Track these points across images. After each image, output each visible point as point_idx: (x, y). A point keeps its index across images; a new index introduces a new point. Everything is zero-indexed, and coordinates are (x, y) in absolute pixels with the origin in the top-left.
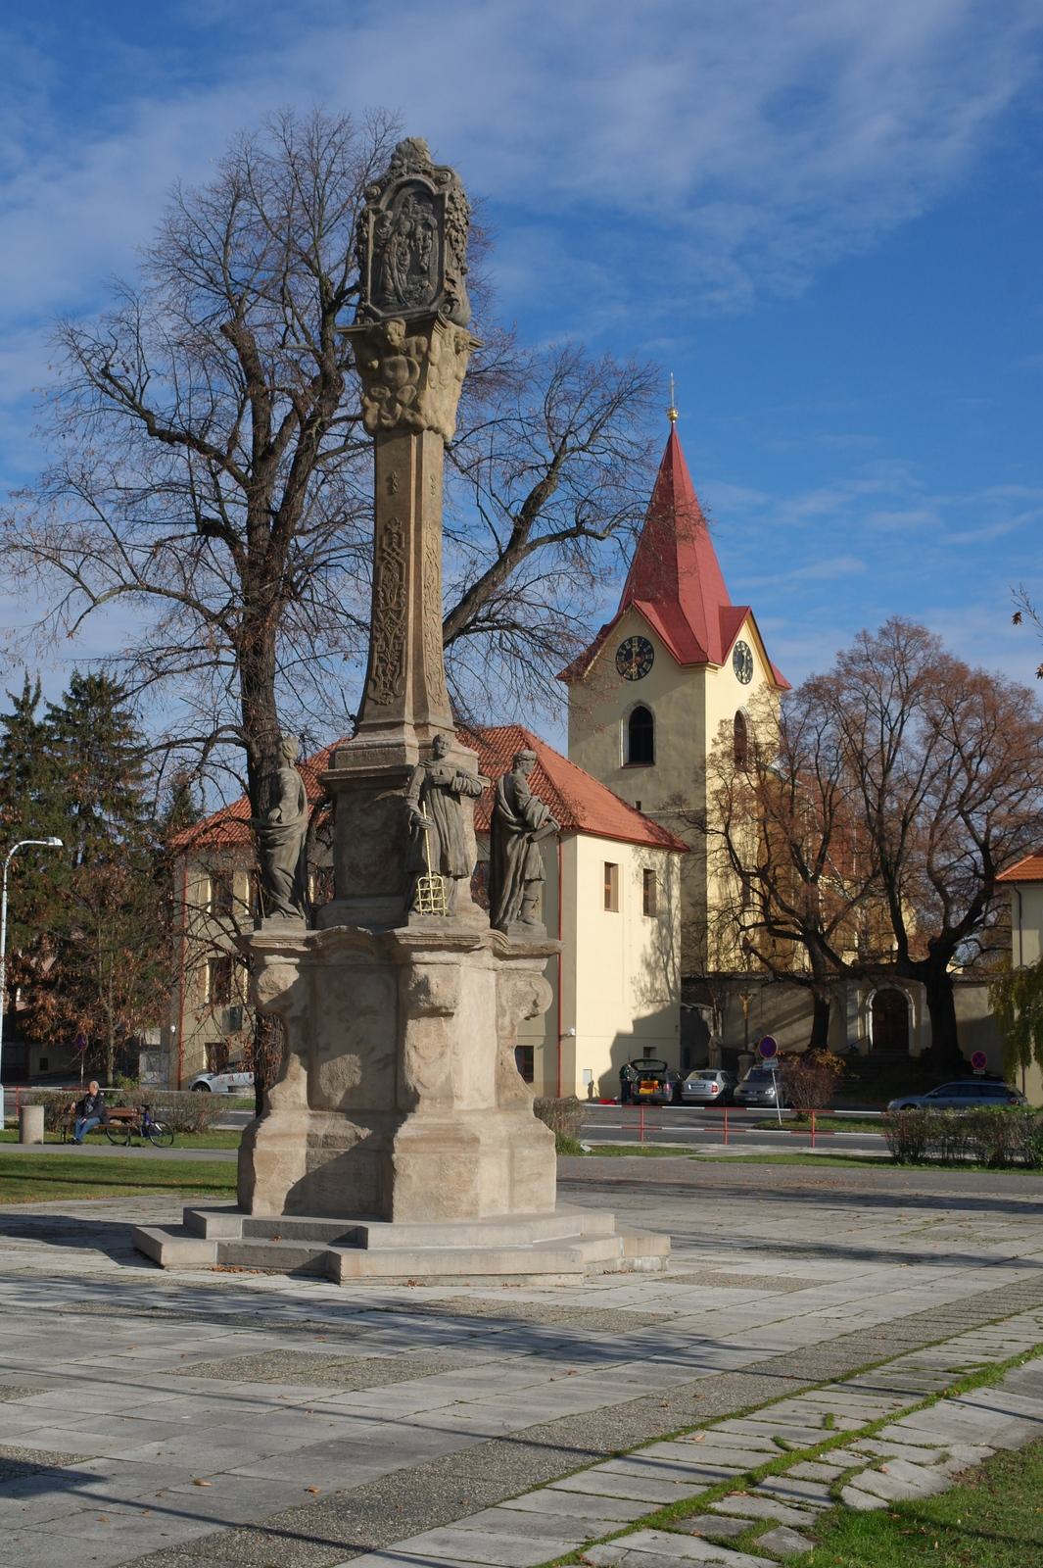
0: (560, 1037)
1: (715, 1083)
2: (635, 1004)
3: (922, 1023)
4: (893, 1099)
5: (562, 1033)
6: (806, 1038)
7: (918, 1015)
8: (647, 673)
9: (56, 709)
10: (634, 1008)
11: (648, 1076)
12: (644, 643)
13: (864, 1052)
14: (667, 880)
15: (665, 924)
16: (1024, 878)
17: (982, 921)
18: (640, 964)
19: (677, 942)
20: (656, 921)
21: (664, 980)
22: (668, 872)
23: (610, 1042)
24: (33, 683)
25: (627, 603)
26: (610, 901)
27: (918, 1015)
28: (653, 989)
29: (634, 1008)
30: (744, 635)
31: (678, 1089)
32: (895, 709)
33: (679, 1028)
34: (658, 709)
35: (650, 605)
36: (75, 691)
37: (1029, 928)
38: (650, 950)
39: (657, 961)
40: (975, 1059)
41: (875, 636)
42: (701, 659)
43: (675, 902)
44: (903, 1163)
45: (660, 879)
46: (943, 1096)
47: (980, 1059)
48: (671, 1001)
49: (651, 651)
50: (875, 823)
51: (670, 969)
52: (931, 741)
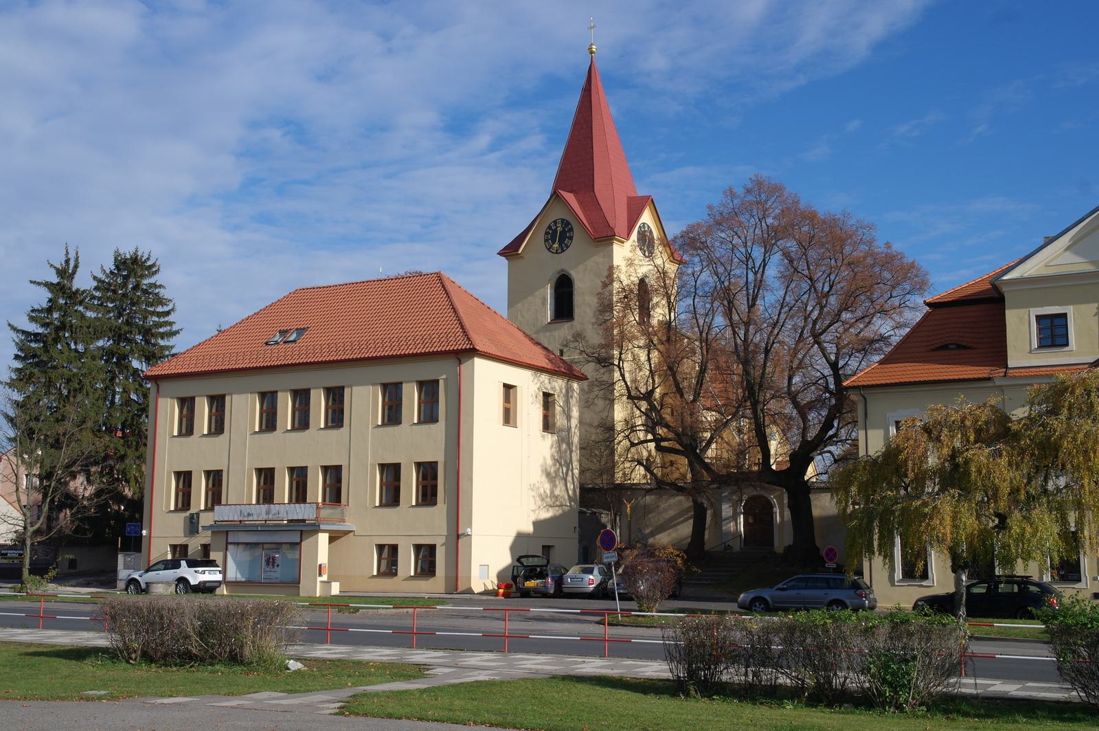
0: (458, 536)
1: (591, 577)
2: (533, 507)
3: (785, 519)
4: (741, 593)
5: (460, 533)
6: (689, 538)
7: (781, 514)
8: (568, 247)
9: (99, 281)
10: (533, 511)
11: (532, 573)
12: (566, 223)
13: (737, 546)
14: (567, 402)
15: (564, 439)
16: (870, 383)
17: (835, 435)
18: (540, 473)
19: (576, 456)
20: (555, 438)
21: (564, 488)
22: (568, 397)
23: (509, 541)
24: (72, 256)
25: (555, 195)
26: (509, 417)
27: (781, 514)
28: (553, 495)
29: (533, 511)
30: (646, 218)
31: (559, 582)
32: (758, 253)
33: (577, 529)
34: (575, 275)
35: (572, 195)
36: (117, 267)
37: (874, 428)
38: (549, 462)
39: (556, 472)
40: (827, 554)
41: (740, 191)
42: (609, 234)
43: (574, 422)
44: (687, 695)
45: (560, 401)
46: (792, 588)
47: (831, 553)
48: (571, 506)
49: (571, 230)
50: (745, 355)
51: (569, 478)
52: (787, 279)
